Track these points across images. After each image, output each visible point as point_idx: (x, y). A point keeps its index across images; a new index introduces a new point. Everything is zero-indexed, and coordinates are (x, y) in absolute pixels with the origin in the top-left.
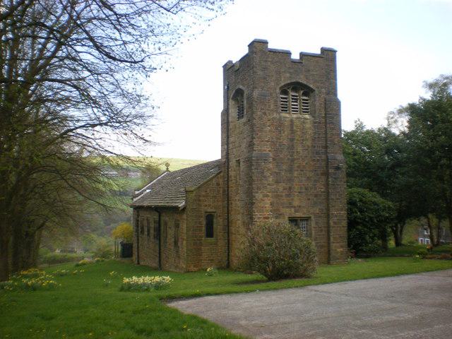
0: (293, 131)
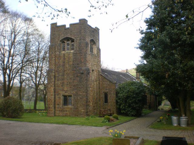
0: (64, 59)
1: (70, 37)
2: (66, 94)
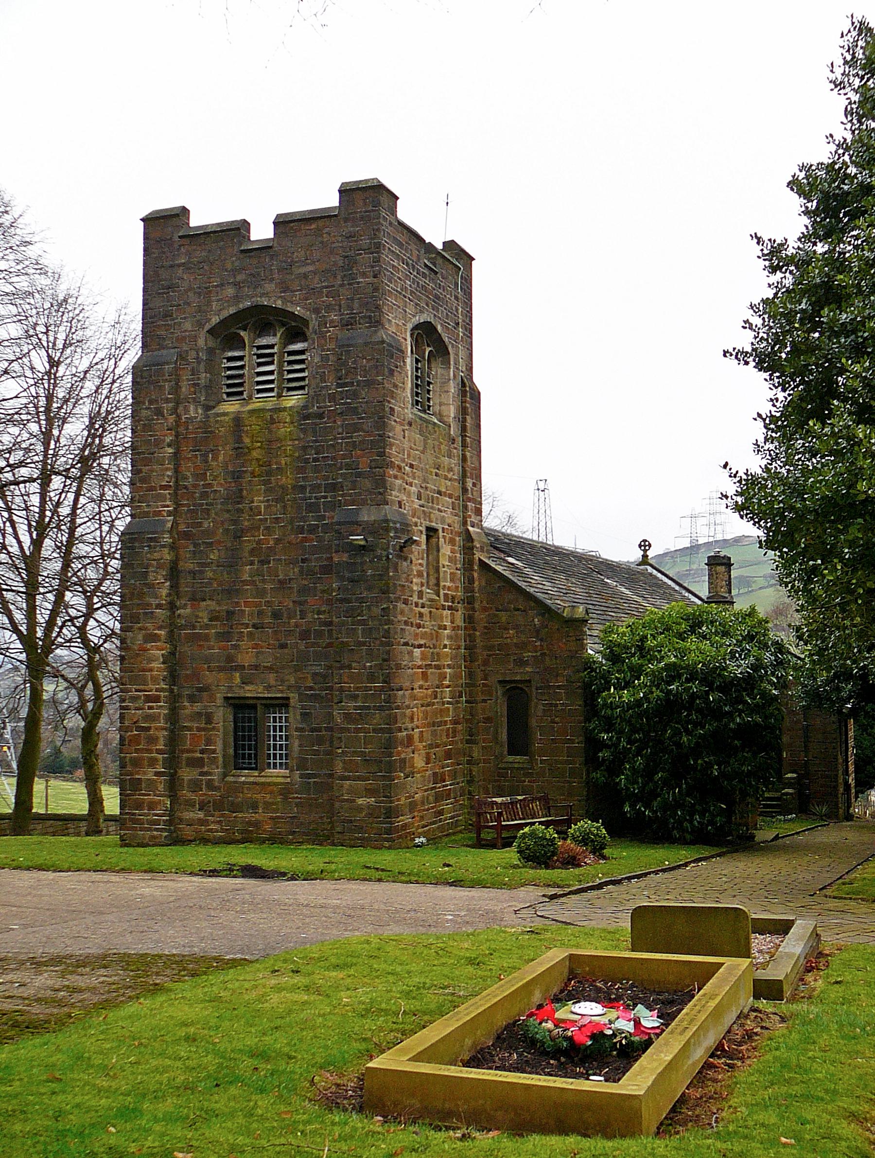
0: (240, 451)
1: (279, 304)
2: (250, 691)
